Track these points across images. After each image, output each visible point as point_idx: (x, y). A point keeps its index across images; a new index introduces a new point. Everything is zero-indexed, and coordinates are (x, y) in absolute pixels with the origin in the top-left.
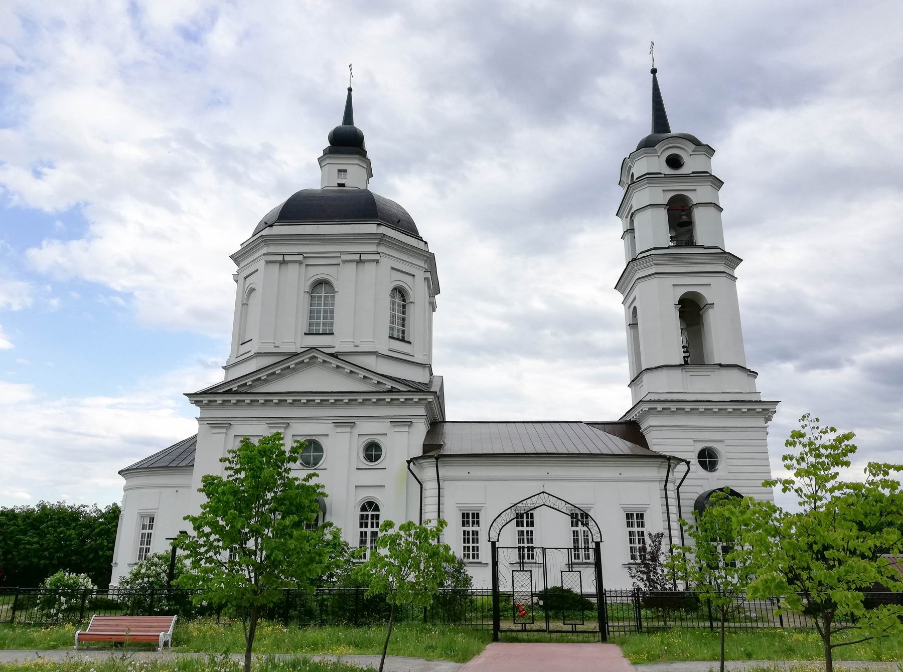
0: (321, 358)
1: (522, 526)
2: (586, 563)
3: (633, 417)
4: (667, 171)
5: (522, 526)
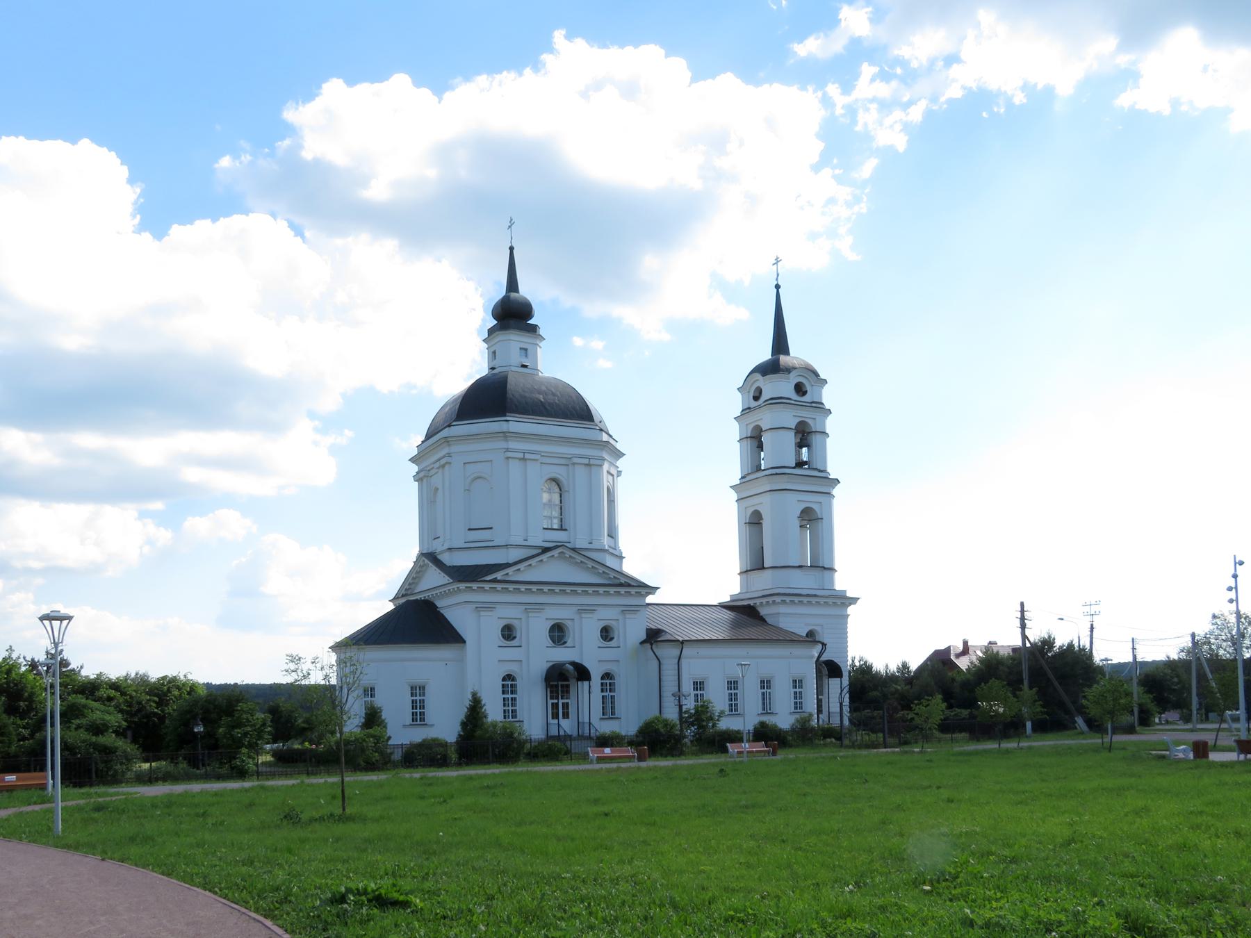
0: (568, 553)
1: (697, 690)
2: (612, 718)
3: (429, 596)
4: (794, 396)
5: (697, 690)
